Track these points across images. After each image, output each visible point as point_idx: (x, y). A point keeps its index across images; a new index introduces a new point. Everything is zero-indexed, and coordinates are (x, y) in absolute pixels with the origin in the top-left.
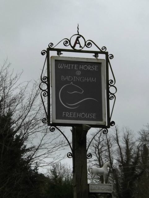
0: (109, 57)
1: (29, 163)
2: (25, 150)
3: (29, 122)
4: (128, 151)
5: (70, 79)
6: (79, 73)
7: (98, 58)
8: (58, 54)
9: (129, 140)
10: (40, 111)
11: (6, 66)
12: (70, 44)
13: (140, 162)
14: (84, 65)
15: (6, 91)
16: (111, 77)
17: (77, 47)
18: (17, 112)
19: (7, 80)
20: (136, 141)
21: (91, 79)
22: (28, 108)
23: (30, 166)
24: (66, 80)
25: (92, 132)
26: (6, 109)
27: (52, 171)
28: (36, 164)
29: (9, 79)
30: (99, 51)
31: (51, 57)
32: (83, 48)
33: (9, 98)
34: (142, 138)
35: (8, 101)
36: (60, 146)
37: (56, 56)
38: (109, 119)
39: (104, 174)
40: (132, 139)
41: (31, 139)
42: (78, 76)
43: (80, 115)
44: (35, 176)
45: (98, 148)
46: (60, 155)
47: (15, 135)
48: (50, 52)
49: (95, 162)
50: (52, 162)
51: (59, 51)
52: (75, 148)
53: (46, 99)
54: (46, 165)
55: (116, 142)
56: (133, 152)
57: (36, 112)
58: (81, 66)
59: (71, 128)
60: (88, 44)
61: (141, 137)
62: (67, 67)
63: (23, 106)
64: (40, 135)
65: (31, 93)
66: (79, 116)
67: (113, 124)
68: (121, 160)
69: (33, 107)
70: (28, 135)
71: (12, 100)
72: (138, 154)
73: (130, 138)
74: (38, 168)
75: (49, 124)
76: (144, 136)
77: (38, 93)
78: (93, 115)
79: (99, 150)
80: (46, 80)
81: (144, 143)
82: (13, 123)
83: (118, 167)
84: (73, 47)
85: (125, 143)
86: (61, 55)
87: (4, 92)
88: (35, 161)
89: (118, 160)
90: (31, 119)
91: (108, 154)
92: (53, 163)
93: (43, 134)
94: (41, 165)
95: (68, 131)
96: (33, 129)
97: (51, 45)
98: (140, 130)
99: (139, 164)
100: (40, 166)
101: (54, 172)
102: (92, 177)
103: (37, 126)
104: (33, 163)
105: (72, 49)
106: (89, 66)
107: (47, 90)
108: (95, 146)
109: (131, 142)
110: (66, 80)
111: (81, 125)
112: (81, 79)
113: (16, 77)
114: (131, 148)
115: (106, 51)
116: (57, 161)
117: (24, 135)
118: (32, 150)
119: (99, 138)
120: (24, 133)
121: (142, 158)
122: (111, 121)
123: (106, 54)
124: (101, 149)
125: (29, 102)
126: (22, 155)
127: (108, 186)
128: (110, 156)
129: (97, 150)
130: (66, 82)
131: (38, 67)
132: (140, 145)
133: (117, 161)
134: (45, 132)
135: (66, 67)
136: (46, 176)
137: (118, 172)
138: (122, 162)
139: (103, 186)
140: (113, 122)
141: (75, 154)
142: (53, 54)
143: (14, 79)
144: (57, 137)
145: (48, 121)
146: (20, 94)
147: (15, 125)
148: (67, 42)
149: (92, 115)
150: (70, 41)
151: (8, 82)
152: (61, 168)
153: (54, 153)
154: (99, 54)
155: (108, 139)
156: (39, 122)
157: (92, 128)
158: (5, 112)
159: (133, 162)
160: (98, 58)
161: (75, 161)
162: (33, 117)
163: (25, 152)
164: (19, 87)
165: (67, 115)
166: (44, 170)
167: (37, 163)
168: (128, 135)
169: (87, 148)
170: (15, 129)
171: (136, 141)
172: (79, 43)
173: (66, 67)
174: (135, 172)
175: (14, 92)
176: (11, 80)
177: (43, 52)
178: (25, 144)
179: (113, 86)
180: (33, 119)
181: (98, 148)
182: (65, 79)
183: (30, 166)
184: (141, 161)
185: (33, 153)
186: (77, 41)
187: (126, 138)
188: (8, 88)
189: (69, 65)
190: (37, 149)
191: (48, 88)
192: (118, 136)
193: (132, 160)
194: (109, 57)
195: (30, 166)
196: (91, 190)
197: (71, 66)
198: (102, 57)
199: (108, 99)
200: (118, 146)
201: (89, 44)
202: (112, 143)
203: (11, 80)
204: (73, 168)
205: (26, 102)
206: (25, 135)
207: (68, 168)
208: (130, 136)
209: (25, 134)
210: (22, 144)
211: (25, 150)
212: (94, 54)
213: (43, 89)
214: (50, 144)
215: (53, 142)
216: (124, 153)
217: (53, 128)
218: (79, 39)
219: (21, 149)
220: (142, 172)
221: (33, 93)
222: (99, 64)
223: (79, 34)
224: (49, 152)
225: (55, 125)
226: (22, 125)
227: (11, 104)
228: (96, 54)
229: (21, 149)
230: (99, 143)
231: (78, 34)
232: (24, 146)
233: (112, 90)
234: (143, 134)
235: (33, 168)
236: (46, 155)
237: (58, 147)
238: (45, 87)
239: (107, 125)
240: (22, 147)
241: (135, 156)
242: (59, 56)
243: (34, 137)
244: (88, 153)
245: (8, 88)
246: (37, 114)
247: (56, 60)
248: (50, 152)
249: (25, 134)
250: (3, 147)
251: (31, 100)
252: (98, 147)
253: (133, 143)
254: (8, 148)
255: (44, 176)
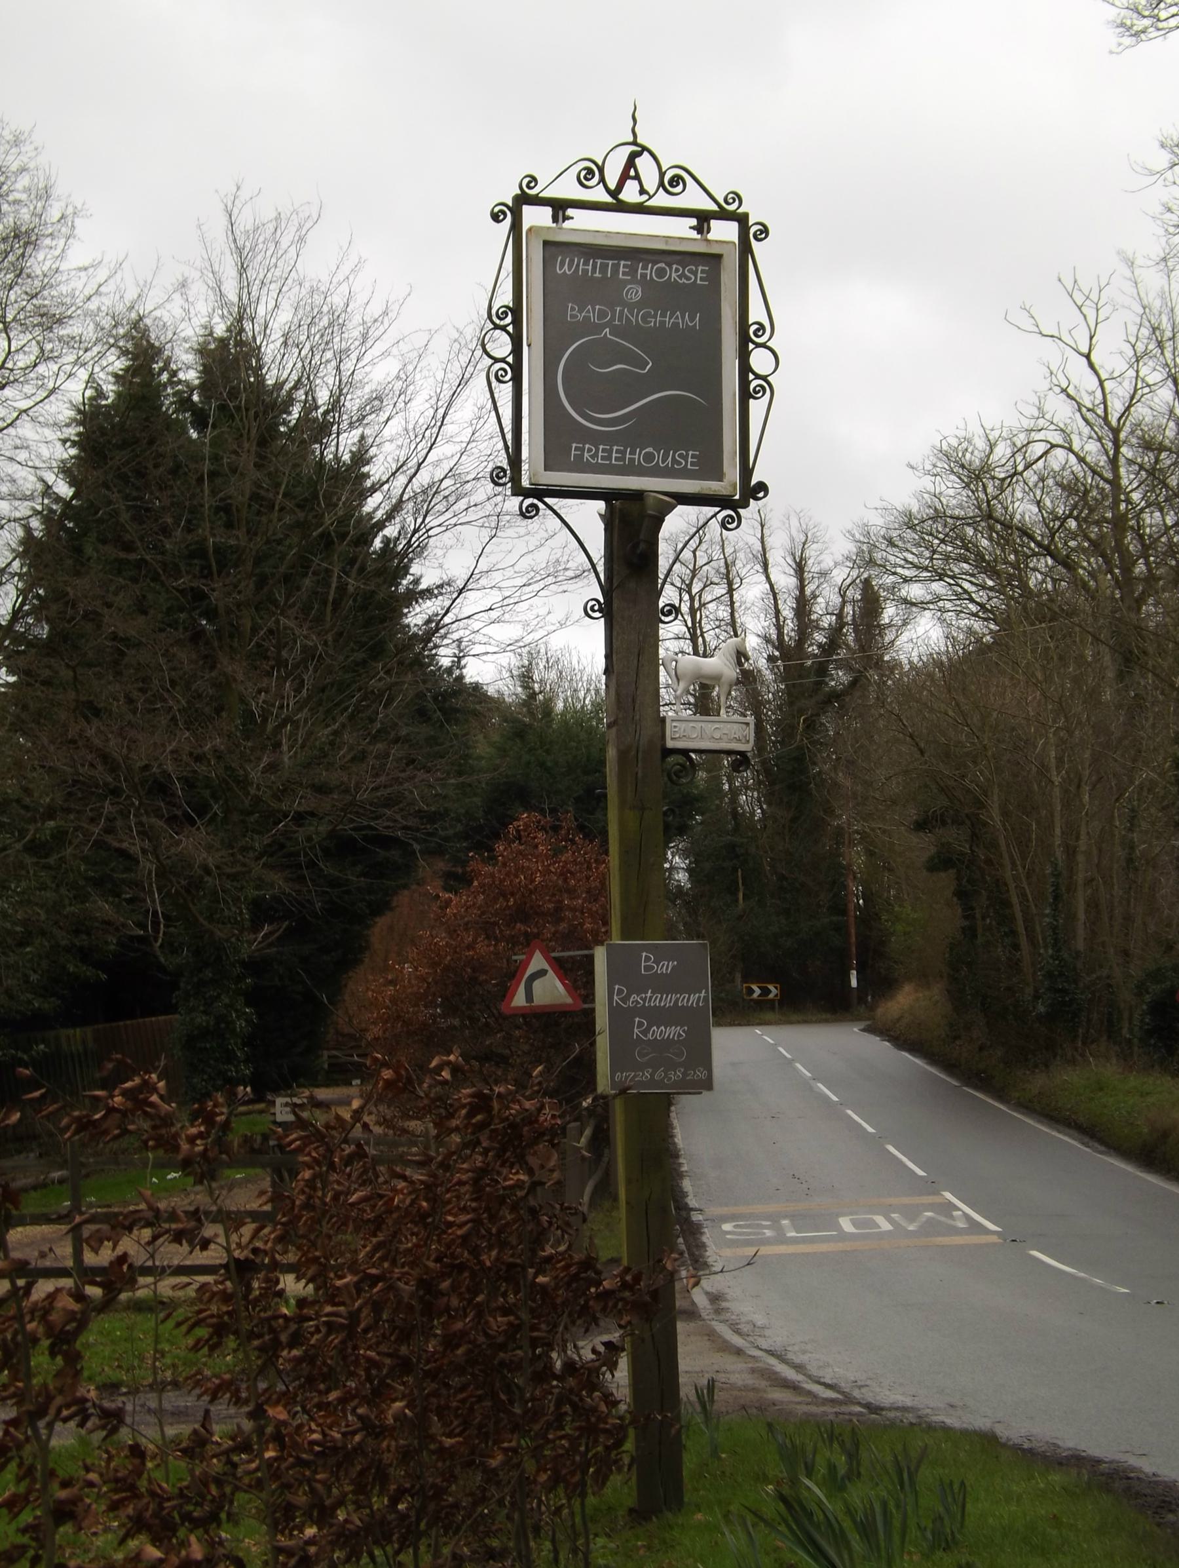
0: (750, 234)
1: (430, 640)
2: (415, 595)
3: (430, 486)
4: (803, 605)
5: (602, 314)
6: (634, 293)
7: (710, 236)
8: (555, 219)
9: (810, 562)
10: (474, 444)
11: (346, 269)
12: (602, 180)
13: (847, 645)
14: (655, 263)
15: (348, 366)
16: (756, 313)
17: (630, 193)
18: (388, 447)
19: (350, 325)
20: (836, 564)
21: (683, 318)
22: (428, 432)
23: (436, 655)
24: (587, 318)
25: (677, 523)
26: (345, 435)
27: (515, 673)
28: (459, 646)
29: (357, 319)
30: (715, 208)
31: (530, 230)
32: (651, 197)
33: (359, 393)
34: (860, 552)
35: (352, 404)
36: (551, 580)
37: (549, 228)
38: (746, 471)
39: (723, 680)
40: (820, 558)
41: (440, 552)
42: (631, 307)
43: (638, 457)
44: (455, 694)
45: (689, 592)
46: (549, 613)
47: (380, 534)
48: (526, 209)
49: (676, 642)
50: (517, 641)
51: (560, 207)
52: (615, 585)
53: (505, 392)
54: (496, 649)
55: (758, 567)
56: (823, 605)
57: (458, 448)
58: (645, 268)
59: (600, 505)
60: (674, 182)
61: (855, 550)
62: (590, 268)
63: (411, 427)
64: (474, 536)
65: (440, 375)
66: (632, 460)
67: (761, 494)
68: (774, 637)
69: (448, 429)
70: (429, 537)
71: (370, 400)
72: (840, 616)
73: (813, 553)
74: (463, 662)
75: (518, 491)
76: (865, 547)
77: (467, 375)
78: (685, 458)
79: (692, 599)
80: (509, 319)
81: (865, 575)
82: (374, 489)
83: (762, 663)
84: (614, 193)
85: (792, 572)
86: (567, 224)
87: (338, 368)
88: (455, 636)
89: (767, 640)
90: (439, 475)
91: (725, 614)
92: (521, 644)
93: (486, 534)
94: (477, 649)
95: (588, 517)
96: (448, 515)
97: (530, 182)
98: (849, 526)
99: (842, 653)
100: (471, 653)
101: (526, 678)
102: (679, 692)
103: (462, 504)
104: (446, 641)
105: (609, 199)
106: (674, 266)
107: (510, 359)
108: (679, 585)
109: (816, 569)
110: (587, 318)
111: (638, 496)
112: (644, 318)
113: (385, 313)
114: (813, 592)
115: (740, 211)
116: (536, 635)
117: (412, 536)
118: (441, 594)
119: (694, 552)
120: (412, 527)
121: (856, 631)
122: (753, 482)
123: (742, 220)
124: (700, 597)
125: (432, 411)
126: (406, 611)
127: (736, 726)
128: (733, 623)
129: (686, 597)
130: (587, 327)
131: (471, 274)
132: (848, 581)
133: (759, 640)
134: (493, 525)
135: (585, 271)
136: (491, 691)
137: (763, 682)
138: (780, 644)
139: (717, 726)
140: (762, 487)
141: (615, 606)
142: (536, 217)
143: (376, 321)
144: (537, 547)
145: (512, 480)
146: (398, 378)
147: (377, 497)
148: (592, 172)
149: (680, 456)
150: (601, 170)
151: (356, 333)
152: (548, 662)
153: (523, 606)
154: (713, 222)
155: (730, 559)
156: (468, 486)
157: (679, 507)
158: (341, 449)
159: (820, 646)
160: (710, 236)
161: (615, 633)
162: (446, 466)
163: (417, 602)
164: (395, 351)
165: (586, 455)
166: (488, 671)
167: (460, 641)
168: (804, 544)
169: (660, 581)
170: (379, 514)
171: (836, 564)
172: (637, 177)
173: (585, 271)
174: (827, 679)
175: (377, 372)
176: (364, 323)
177: (496, 210)
178: (415, 569)
179: (764, 345)
180: (445, 477)
181: (689, 592)
182: (580, 317)
183: (434, 652)
184: (851, 638)
185: (447, 603)
186: (629, 171)
187: (798, 554)
188: (354, 357)
189: (599, 261)
190: (461, 592)
191: (517, 351)
192: (768, 547)
193: (820, 637)
194: (750, 234)
195: (434, 652)
196: (672, 739)
197: (604, 268)
198: (724, 232)
199: (746, 395)
200: (767, 586)
201: (676, 180)
202: (743, 573)
203: (364, 323)
204: (606, 657)
205: (420, 409)
206: (417, 535)
207: (575, 662)
208: (814, 546)
209: (416, 531)
210: (406, 570)
211: (415, 595)
212: (693, 222)
213: (498, 354)
214: (509, 573)
215: (523, 564)
216: (787, 612)
217: (533, 505)
218: (638, 161)
219: (401, 589)
220: (854, 683)
221: (450, 375)
222: (713, 260)
223: (639, 141)
224: (505, 602)
225: (540, 493)
226: (406, 497)
227: (364, 417)
228: (703, 219)
229: (401, 589)
230: (694, 573)
231: (635, 143)
232: (412, 578)
233: (760, 361)
234: (862, 539)
235: (446, 662)
236: (494, 614)
237: (542, 584)
238: (502, 346)
239: (737, 497)
240: (405, 582)
241: (826, 622)
242: (561, 228)
243: (449, 543)
244: (662, 603)
245: (354, 357)
246: (464, 457)
247: (546, 244)
248: (512, 601)
249: (416, 531)
250: (335, 579)
251: (440, 404)
252: (690, 586)
253: (824, 574)
254: (352, 583)
255: (485, 694)
